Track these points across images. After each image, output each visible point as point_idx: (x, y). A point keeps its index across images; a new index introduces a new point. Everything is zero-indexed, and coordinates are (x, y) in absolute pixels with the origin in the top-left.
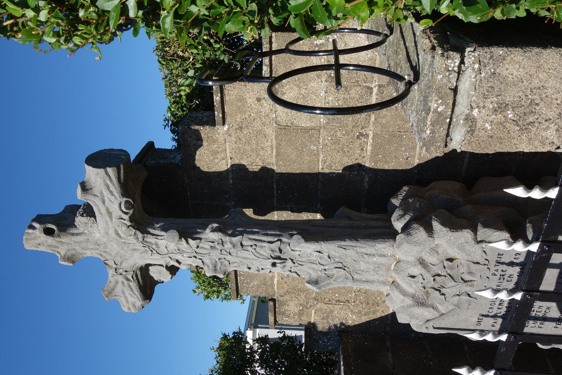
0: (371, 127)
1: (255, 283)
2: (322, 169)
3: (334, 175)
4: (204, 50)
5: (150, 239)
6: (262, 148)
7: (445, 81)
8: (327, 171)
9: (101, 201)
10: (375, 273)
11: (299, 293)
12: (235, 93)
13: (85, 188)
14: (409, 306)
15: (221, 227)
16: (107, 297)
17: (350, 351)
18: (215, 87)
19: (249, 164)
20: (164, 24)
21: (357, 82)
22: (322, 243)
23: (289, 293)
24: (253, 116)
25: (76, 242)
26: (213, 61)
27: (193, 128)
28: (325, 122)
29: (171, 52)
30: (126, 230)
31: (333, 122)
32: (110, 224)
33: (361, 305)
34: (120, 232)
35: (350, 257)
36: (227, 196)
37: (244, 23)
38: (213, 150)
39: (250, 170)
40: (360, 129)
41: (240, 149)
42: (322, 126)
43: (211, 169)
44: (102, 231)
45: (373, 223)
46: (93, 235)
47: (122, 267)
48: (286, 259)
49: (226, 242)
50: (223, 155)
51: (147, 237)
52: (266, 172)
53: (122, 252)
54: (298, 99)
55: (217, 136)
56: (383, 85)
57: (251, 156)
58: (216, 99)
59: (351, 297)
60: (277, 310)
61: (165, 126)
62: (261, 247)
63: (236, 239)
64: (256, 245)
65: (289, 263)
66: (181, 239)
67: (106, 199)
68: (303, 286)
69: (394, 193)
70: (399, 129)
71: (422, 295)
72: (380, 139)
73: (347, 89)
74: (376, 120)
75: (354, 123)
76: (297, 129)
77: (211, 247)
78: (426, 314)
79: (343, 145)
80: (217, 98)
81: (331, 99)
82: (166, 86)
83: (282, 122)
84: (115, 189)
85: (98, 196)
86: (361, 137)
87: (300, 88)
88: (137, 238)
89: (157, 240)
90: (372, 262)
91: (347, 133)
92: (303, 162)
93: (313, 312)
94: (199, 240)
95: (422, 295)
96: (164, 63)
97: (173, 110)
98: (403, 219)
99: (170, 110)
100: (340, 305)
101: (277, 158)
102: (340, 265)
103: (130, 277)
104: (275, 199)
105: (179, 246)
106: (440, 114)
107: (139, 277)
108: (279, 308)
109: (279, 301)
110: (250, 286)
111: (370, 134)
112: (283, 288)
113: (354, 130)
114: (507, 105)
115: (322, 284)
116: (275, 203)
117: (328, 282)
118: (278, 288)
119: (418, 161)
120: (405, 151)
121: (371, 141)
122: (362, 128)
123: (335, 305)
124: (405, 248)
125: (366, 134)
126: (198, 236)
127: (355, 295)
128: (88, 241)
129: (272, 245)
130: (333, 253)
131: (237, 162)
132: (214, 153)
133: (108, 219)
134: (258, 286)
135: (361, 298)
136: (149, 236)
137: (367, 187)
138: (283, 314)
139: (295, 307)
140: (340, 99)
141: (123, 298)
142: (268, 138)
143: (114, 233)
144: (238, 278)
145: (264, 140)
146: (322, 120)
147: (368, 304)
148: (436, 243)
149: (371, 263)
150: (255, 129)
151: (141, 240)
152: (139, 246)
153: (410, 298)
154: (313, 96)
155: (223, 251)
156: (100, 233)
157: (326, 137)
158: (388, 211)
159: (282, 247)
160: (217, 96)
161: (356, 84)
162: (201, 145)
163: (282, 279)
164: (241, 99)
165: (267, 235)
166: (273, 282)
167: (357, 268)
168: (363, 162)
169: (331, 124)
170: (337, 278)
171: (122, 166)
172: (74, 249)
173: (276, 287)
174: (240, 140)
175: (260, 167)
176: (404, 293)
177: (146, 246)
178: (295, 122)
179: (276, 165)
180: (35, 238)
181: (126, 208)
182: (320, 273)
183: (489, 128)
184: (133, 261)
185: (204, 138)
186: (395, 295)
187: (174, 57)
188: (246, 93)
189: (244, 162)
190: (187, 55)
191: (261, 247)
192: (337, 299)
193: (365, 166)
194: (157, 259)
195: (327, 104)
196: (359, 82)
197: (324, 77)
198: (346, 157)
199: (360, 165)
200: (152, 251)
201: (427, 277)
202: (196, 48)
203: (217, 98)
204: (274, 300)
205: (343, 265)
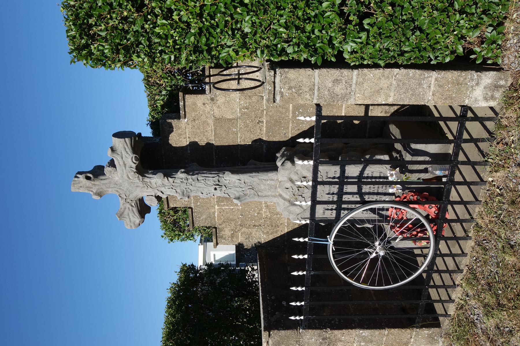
0: (264, 117)
1: (204, 217)
2: (240, 142)
4: (172, 80)
5: (146, 180)
6: (206, 131)
7: (270, 79)
8: (243, 143)
9: (121, 158)
13: (113, 150)
14: (288, 207)
15: (186, 171)
17: (263, 255)
20: (182, 62)
21: (255, 93)
22: (241, 175)
25: (103, 184)
26: (176, 86)
29: (152, 81)
31: (244, 115)
32: (125, 171)
33: (268, 227)
35: (256, 182)
36: (186, 161)
37: (207, 62)
38: (179, 133)
44: (120, 176)
45: (269, 166)
46: (114, 178)
48: (222, 186)
49: (189, 179)
50: (184, 136)
52: (209, 145)
53: (130, 188)
55: (181, 125)
61: (148, 125)
62: (208, 180)
63: (194, 177)
65: (224, 188)
67: (124, 156)
69: (278, 152)
74: (266, 113)
77: (181, 182)
78: (297, 210)
79: (251, 127)
82: (149, 101)
84: (129, 150)
87: (226, 97)
89: (150, 180)
90: (268, 185)
92: (229, 138)
93: (240, 234)
94: (174, 178)
96: (148, 87)
97: (152, 114)
98: (281, 160)
99: (151, 114)
102: (251, 187)
103: (133, 205)
104: (214, 161)
105: (163, 182)
106: (270, 90)
107: (138, 205)
108: (219, 233)
110: (201, 219)
112: (221, 219)
113: (256, 119)
114: (292, 87)
115: (242, 199)
116: (215, 164)
117: (245, 198)
118: (218, 219)
120: (284, 130)
122: (260, 118)
125: (262, 121)
126: (174, 176)
127: (264, 221)
128: (110, 183)
129: (214, 179)
130: (246, 181)
131: (192, 140)
133: (124, 168)
134: (206, 219)
136: (146, 178)
137: (265, 151)
138: (222, 237)
143: (126, 176)
144: (194, 214)
146: (238, 114)
147: (272, 226)
148: (296, 169)
151: (141, 180)
152: (140, 184)
154: (233, 102)
157: (241, 124)
158: (275, 159)
159: (220, 179)
160: (182, 102)
161: (255, 94)
162: (173, 131)
163: (220, 213)
164: (195, 104)
165: (211, 174)
167: (260, 189)
170: (250, 195)
171: (133, 137)
172: (102, 188)
173: (216, 219)
175: (206, 143)
176: (284, 199)
178: (224, 116)
179: (215, 141)
180: (79, 183)
181: (136, 160)
182: (240, 193)
183: (288, 95)
184: (136, 194)
187: (155, 84)
188: (197, 101)
189: (196, 140)
190: (161, 82)
191: (208, 180)
192: (254, 224)
194: (150, 192)
199: (260, 139)
202: (167, 79)
204: (216, 228)
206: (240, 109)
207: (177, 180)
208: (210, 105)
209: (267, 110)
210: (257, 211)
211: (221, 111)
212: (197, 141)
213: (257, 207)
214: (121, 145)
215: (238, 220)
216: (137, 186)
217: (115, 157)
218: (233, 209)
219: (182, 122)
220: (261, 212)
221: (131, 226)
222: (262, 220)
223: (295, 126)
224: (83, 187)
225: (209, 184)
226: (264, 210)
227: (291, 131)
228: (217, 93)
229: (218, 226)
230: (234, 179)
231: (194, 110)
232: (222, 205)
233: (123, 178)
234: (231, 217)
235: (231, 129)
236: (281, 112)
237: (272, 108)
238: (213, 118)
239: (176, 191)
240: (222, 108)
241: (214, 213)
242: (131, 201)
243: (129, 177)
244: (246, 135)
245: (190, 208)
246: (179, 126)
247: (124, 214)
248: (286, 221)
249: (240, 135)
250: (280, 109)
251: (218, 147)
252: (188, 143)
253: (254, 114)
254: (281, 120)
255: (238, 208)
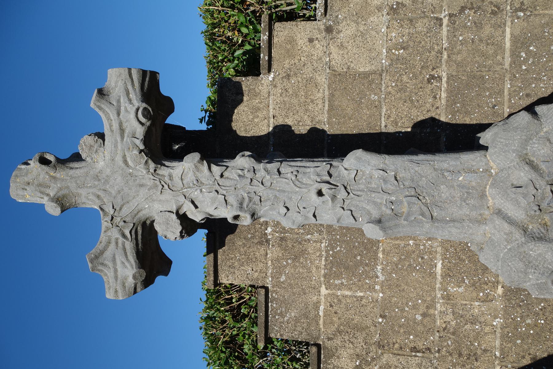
2: (386, 126)
3: (401, 135)
6: (312, 101)
8: (391, 129)
9: (115, 112)
10: (464, 204)
11: (356, 332)
12: (285, 34)
16: (91, 262)
18: (264, 25)
19: (295, 123)
21: (424, 12)
22: (387, 156)
23: (340, 332)
24: (303, 61)
25: (72, 177)
27: (233, 79)
28: (387, 64)
30: (137, 157)
31: (396, 64)
33: (450, 358)
34: (129, 160)
39: (297, 132)
40: (431, 70)
41: (285, 104)
42: (384, 69)
43: (249, 131)
44: (107, 158)
47: (120, 215)
48: (338, 186)
51: (160, 169)
54: (356, 37)
55: (260, 88)
56: (454, 15)
57: (298, 112)
58: (263, 38)
59: (433, 342)
60: (322, 366)
64: (298, 171)
66: (203, 161)
67: (122, 108)
68: (361, 320)
70: (479, 68)
71: (539, 229)
72: (457, 82)
73: (412, 21)
74: (449, 57)
75: (423, 63)
76: (355, 75)
77: (239, 176)
79: (411, 92)
80: (264, 38)
81: (394, 35)
83: (337, 67)
85: (114, 105)
86: (432, 81)
87: (358, 24)
88: (148, 169)
90: (458, 186)
91: (415, 76)
92: (361, 118)
94: (225, 168)
95: (539, 229)
100: (418, 356)
101: (330, 114)
105: (199, 175)
107: (140, 237)
109: (326, 348)
110: (286, 319)
111: (444, 76)
112: (332, 323)
113: (424, 72)
115: (387, 224)
118: (324, 323)
119: (508, 110)
120: (490, 96)
121: (445, 85)
122: (433, 69)
123: (409, 358)
124: (502, 140)
125: (439, 77)
126: (224, 164)
127: (440, 337)
132: (255, 111)
133: (119, 139)
134: (297, 320)
135: (449, 343)
139: (349, 361)
140: (404, 34)
141: (112, 270)
142: (319, 88)
144: (270, 304)
145: (315, 91)
146: (384, 61)
147: (460, 355)
148: (545, 130)
149: (456, 187)
150: (305, 77)
151: (152, 170)
152: (149, 180)
153: (520, 231)
154: (373, 33)
155: (254, 181)
156: (104, 160)
159: (332, 171)
160: (265, 35)
162: (242, 101)
164: (291, 41)
166: (318, 313)
168: (437, 114)
169: (395, 66)
172: (68, 187)
173: (321, 322)
174: (287, 91)
175: (308, 128)
176: (511, 221)
177: (157, 179)
178: (352, 65)
179: (328, 124)
182: (384, 208)
185: (245, 91)
186: (497, 227)
188: (297, 33)
189: (289, 122)
192: (412, 345)
193: (439, 121)
195: (390, 42)
196: (426, 13)
197: (385, 10)
198: (415, 109)
199: (433, 119)
200: (163, 186)
201: (540, 185)
203: (264, 38)
204: (318, 346)
205: (416, 193)
206: (389, 50)
207: (232, 173)
208: (324, 43)
209: (451, 50)
210: (422, 309)
211: (346, 56)
212: (290, 123)
213: (421, 297)
214: (120, 84)
215: (372, 329)
216: (141, 186)
217: (104, 111)
218: (362, 298)
219: (263, 82)
220: (431, 311)
221: (116, 291)
222: (433, 335)
223: (520, 88)
224: (33, 184)
225: (304, 184)
226: (438, 306)
227: (510, 100)
228: (340, 16)
229: (324, 342)
230: (369, 168)
231: (289, 54)
232: (336, 285)
233: (114, 165)
234: (357, 319)
235: (366, 95)
236: (483, 55)
237: (462, 44)
238: (328, 71)
239: (226, 201)
240: (349, 48)
241: (317, 308)
242: (125, 222)
243: (125, 162)
244: (400, 110)
245: (263, 287)
246: (256, 89)
247: (104, 256)
248: (498, 343)
249: (387, 111)
250: (483, 47)
251: (335, 137)
252: (271, 129)
253: (420, 60)
254: (484, 74)
255: (375, 295)
